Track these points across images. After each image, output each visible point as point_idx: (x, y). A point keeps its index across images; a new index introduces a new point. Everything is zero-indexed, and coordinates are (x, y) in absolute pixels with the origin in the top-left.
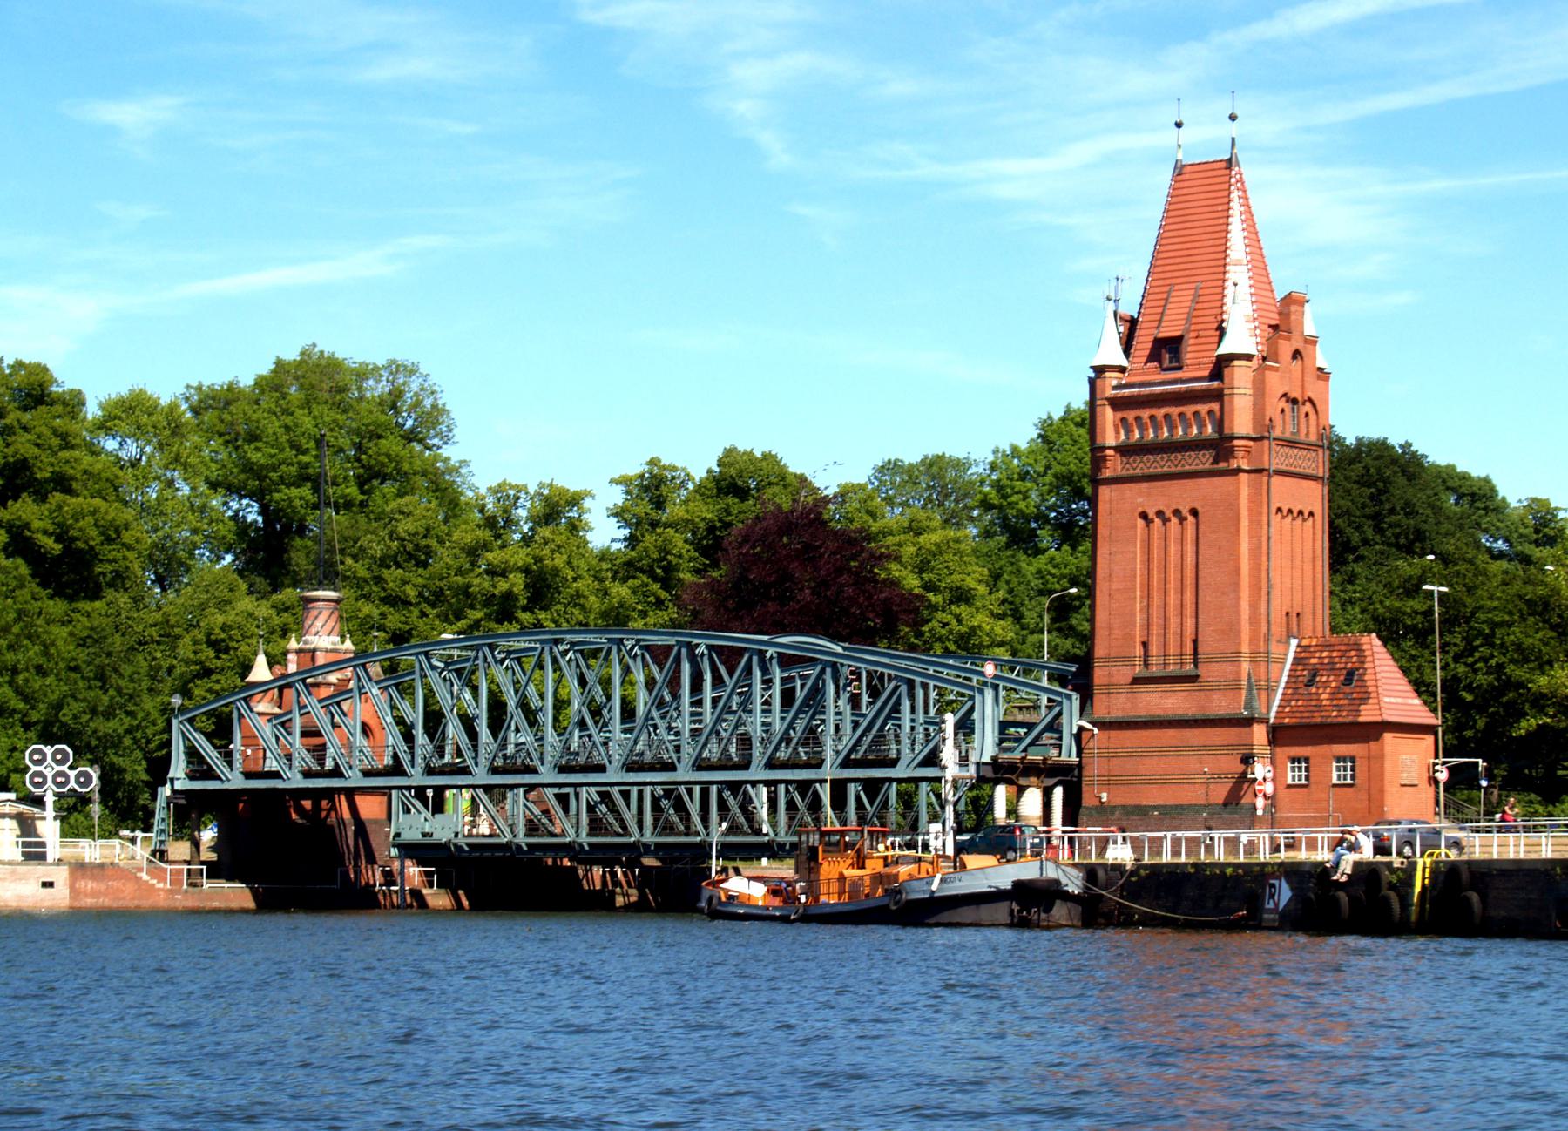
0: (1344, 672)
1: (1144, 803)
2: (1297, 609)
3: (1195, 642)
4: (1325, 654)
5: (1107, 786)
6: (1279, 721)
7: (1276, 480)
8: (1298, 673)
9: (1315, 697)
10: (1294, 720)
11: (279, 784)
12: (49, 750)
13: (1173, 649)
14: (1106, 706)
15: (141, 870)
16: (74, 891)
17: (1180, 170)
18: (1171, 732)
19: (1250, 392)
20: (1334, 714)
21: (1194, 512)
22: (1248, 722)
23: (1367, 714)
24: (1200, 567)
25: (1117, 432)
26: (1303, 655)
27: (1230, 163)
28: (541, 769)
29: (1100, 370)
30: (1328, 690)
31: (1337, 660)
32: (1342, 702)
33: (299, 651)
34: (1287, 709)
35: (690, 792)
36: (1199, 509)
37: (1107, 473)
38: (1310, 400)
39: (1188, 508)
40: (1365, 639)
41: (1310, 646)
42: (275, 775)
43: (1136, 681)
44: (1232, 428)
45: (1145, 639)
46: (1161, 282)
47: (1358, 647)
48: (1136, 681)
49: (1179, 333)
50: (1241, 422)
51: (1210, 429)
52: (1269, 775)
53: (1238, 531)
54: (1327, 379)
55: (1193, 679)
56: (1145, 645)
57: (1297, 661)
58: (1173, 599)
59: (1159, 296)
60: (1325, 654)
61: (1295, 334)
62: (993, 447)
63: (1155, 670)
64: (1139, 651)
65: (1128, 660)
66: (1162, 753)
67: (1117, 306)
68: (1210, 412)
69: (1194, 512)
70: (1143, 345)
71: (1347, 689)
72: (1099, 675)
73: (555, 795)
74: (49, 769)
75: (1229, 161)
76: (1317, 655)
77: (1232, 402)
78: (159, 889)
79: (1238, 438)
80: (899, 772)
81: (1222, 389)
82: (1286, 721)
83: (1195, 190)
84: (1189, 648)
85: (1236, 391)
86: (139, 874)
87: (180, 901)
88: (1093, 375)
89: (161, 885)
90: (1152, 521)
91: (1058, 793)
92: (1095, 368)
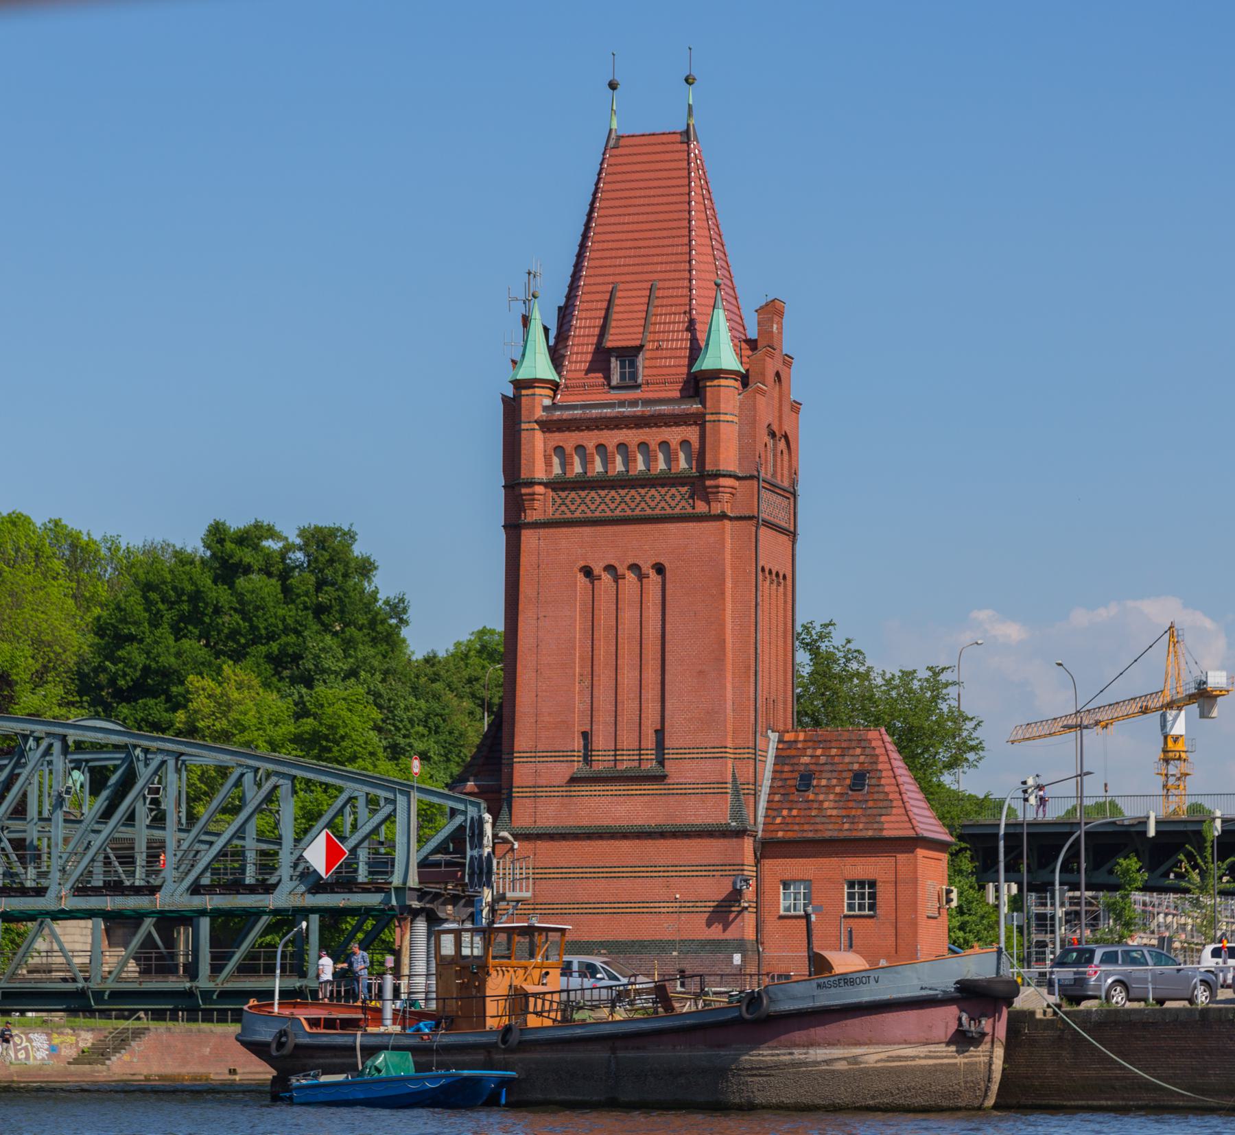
1: (586, 939)
2: (773, 696)
3: (660, 733)
6: (768, 835)
7: (764, 533)
8: (785, 776)
13: (628, 740)
14: (524, 814)
17: (614, 144)
20: (846, 826)
21: (660, 569)
23: (892, 828)
24: (668, 637)
25: (549, 464)
26: (788, 753)
30: (832, 797)
31: (837, 760)
34: (778, 820)
36: (667, 565)
37: (531, 516)
38: (786, 437)
39: (650, 563)
40: (872, 734)
41: (796, 742)
43: (573, 780)
44: (716, 461)
45: (587, 728)
48: (573, 780)
50: (727, 457)
51: (683, 464)
53: (723, 593)
55: (661, 778)
56: (585, 735)
58: (628, 677)
60: (819, 752)
63: (599, 767)
64: (578, 743)
65: (562, 755)
66: (612, 874)
68: (685, 443)
69: (660, 569)
70: (580, 351)
71: (858, 796)
72: (522, 773)
75: (687, 133)
79: (724, 476)
80: (161, 901)
81: (704, 415)
82: (780, 834)
84: (650, 741)
85: (722, 417)
90: (599, 578)
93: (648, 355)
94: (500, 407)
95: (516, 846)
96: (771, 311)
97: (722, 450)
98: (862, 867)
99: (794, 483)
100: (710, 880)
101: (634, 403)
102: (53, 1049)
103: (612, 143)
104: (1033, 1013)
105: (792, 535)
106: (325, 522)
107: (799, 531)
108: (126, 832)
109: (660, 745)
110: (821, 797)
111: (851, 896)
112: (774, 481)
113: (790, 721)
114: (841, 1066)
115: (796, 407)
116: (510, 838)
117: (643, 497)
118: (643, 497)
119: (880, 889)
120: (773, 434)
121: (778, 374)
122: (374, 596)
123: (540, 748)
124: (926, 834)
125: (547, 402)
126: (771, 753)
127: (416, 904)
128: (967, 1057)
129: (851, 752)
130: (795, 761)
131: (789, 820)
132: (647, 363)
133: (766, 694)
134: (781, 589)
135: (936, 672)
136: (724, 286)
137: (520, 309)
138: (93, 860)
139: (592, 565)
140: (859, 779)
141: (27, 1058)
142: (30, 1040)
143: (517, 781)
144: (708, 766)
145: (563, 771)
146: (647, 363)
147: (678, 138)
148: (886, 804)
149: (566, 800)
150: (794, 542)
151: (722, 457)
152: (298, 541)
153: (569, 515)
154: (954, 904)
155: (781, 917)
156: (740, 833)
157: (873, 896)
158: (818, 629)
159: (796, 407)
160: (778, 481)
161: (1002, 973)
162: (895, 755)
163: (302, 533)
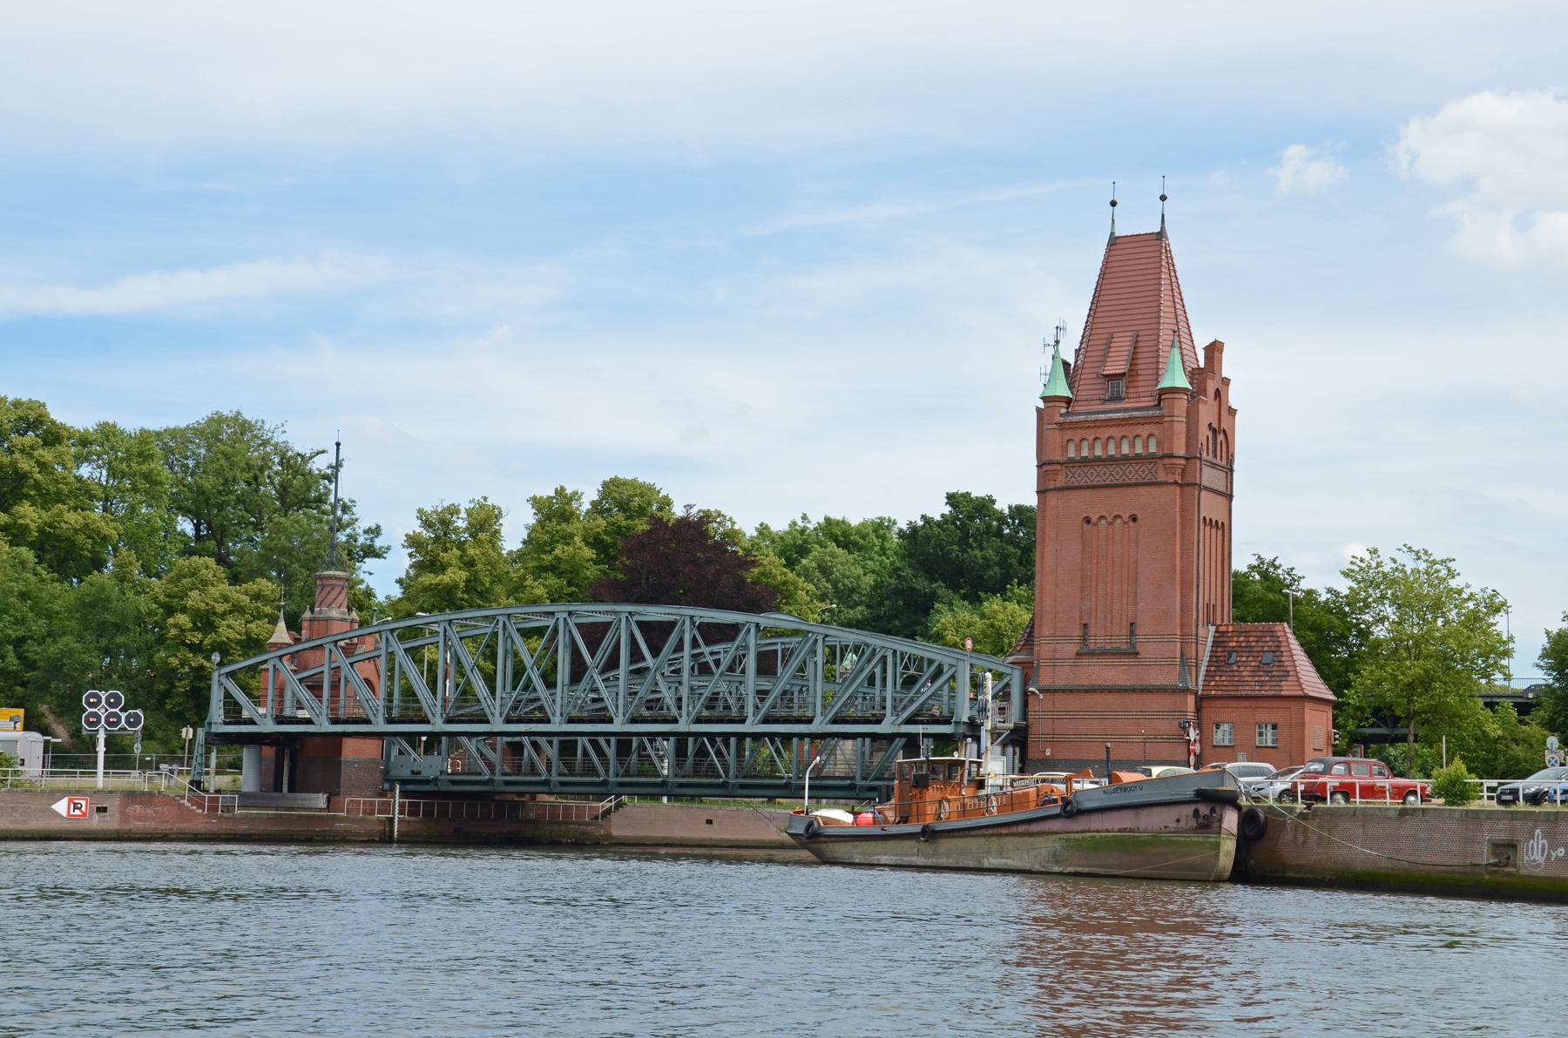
4: (1242, 639)
5: (1051, 742)
6: (1206, 693)
7: (1204, 493)
9: (1237, 674)
12: (103, 695)
15: (183, 797)
16: (124, 816)
17: (1114, 241)
18: (1110, 698)
22: (1185, 691)
26: (1222, 639)
27: (1161, 235)
30: (1248, 668)
31: (1253, 644)
32: (1263, 678)
34: (1213, 683)
35: (608, 742)
38: (1224, 431)
41: (1227, 632)
42: (309, 722)
47: (1272, 633)
52: (1198, 738)
57: (1216, 643)
59: (1096, 337)
60: (1242, 639)
61: (1217, 377)
62: (1505, 594)
67: (1057, 351)
74: (103, 710)
76: (1235, 639)
77: (1172, 428)
78: (199, 814)
82: (1213, 692)
86: (181, 801)
88: (1041, 405)
91: (1017, 750)
92: (1045, 399)
95: (1041, 697)
97: (1175, 440)
99: (1230, 461)
100: (1165, 721)
105: (1230, 497)
108: (765, 684)
110: (1242, 669)
112: (1214, 461)
116: (1037, 692)
117: (1124, 472)
118: (1124, 472)
120: (1214, 431)
124: (1311, 694)
125: (1063, 411)
126: (1210, 639)
129: (1263, 639)
130: (1226, 644)
131: (1219, 683)
133: (1207, 601)
134: (1220, 532)
136: (1181, 333)
137: (1051, 351)
138: (617, 707)
139: (1091, 516)
147: (1155, 236)
148: (1285, 674)
151: (1175, 445)
153: (1115, 482)
156: (1185, 691)
159: (1232, 412)
160: (1218, 461)
161: (344, 739)
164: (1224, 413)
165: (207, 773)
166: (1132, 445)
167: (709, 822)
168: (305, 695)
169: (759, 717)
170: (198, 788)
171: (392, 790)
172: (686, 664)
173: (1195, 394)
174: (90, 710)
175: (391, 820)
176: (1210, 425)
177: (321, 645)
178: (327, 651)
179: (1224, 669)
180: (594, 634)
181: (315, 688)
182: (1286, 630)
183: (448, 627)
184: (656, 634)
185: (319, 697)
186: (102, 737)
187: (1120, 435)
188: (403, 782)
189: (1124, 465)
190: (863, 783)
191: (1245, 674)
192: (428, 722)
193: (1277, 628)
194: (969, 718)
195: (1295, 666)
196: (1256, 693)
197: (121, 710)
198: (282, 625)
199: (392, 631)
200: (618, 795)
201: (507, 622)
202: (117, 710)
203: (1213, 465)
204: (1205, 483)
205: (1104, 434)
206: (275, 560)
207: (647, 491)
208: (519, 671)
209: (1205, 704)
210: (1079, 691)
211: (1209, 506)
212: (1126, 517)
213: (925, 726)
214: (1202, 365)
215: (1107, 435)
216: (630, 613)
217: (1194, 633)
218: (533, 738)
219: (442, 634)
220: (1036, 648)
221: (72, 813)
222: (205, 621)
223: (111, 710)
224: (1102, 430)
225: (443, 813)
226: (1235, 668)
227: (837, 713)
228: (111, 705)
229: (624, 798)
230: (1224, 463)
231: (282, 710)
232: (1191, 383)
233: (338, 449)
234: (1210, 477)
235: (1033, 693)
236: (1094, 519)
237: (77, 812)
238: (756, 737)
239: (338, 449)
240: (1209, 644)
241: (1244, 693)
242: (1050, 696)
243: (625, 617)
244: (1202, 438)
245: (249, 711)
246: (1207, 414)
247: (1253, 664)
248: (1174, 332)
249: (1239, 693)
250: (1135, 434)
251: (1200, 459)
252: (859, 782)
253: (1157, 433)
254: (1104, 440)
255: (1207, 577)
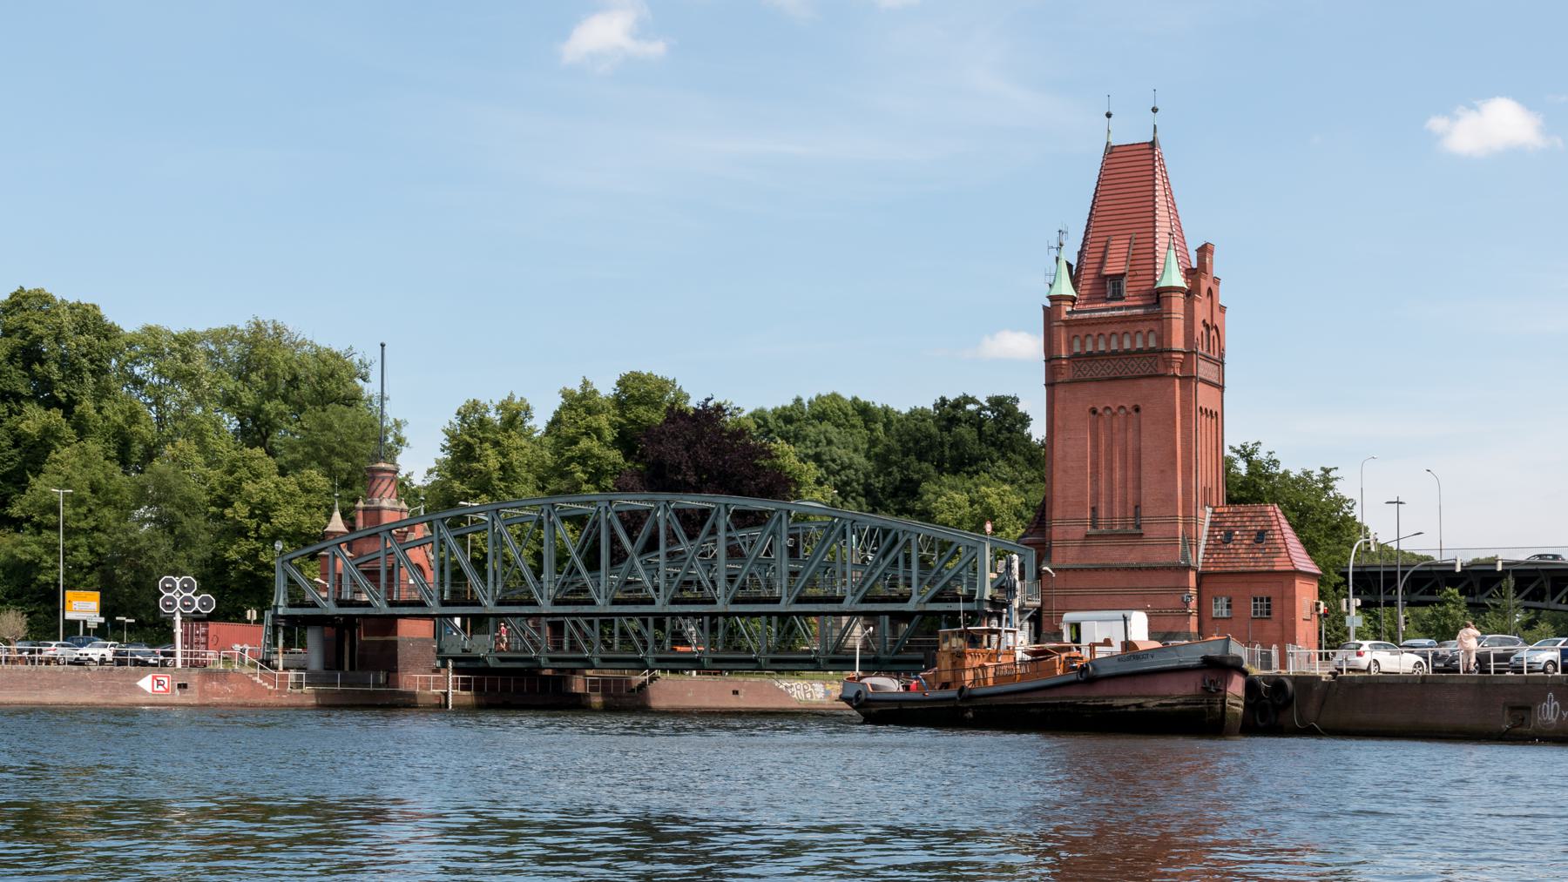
0: (1255, 533)
6: (1205, 569)
7: (1200, 385)
10: (1218, 569)
11: (370, 611)
12: (178, 581)
17: (1111, 151)
19: (1182, 317)
23: (1280, 565)
27: (1153, 145)
28: (598, 601)
29: (1056, 300)
33: (365, 510)
34: (1211, 560)
38: (1216, 328)
42: (368, 604)
46: (1100, 234)
47: (1264, 514)
49: (1122, 272)
53: (1175, 422)
54: (1224, 312)
56: (1093, 509)
57: (1213, 524)
59: (1100, 244)
60: (1236, 519)
61: (1209, 277)
65: (1080, 521)
73: (549, 622)
74: (178, 595)
76: (1231, 519)
77: (1170, 325)
78: (270, 691)
83: (1125, 165)
86: (254, 679)
87: (285, 699)
88: (1048, 304)
89: (271, 687)
91: (1033, 624)
92: (1051, 298)
93: (1129, 279)
94: (1042, 312)
96: (1204, 250)
98: (1261, 590)
99: (1222, 355)
101: (1120, 308)
102: (827, 693)
103: (1108, 151)
104: (1320, 677)
105: (1221, 388)
106: (999, 393)
107: (1226, 385)
109: (1137, 515)
110: (1237, 547)
111: (1256, 606)
112: (1208, 354)
113: (1220, 501)
114: (1133, 709)
115: (1223, 309)
119: (1273, 602)
120: (1207, 326)
121: (1210, 289)
122: (1030, 436)
123: (1068, 517)
124: (1301, 569)
125: (1069, 309)
126: (1208, 520)
127: (989, 610)
128: (186, 697)
132: (1129, 284)
134: (1214, 420)
135: (1327, 471)
136: (1177, 234)
137: (1054, 253)
140: (1261, 536)
141: (812, 697)
142: (813, 687)
143: (1054, 537)
144: (1167, 527)
145: (1079, 531)
146: (1129, 284)
147: (1148, 146)
148: (1276, 550)
149: (1083, 548)
150: (1223, 392)
152: (987, 404)
153: (1082, 377)
154: (1322, 611)
155: (1214, 618)
157: (1268, 606)
158: (1251, 447)
159: (1223, 309)
160: (1211, 355)
161: (399, 620)
162: (1283, 521)
163: (989, 400)
164: (1216, 310)
165: (276, 653)
166: (1133, 341)
167: (736, 692)
168: (363, 581)
169: (792, 598)
170: (268, 665)
171: (445, 666)
172: (721, 550)
173: (1189, 294)
174: (166, 594)
175: (446, 695)
176: (1204, 321)
177: (376, 534)
178: (382, 539)
179: (1221, 547)
180: (633, 521)
181: (372, 575)
182: (1274, 510)
183: (495, 516)
184: (693, 522)
185: (378, 587)
186: (178, 618)
187: (1122, 331)
188: (455, 659)
189: (1151, 357)
190: (886, 656)
191: (1240, 551)
192: (480, 605)
193: (1269, 508)
194: (991, 596)
195: (1285, 544)
196: (1252, 569)
197: (195, 594)
198: (337, 515)
199: (443, 520)
200: (651, 670)
201: (552, 512)
202: (190, 594)
203: (1207, 359)
204: (1200, 375)
205: (1108, 330)
206: (320, 455)
207: (663, 385)
208: (562, 558)
209: (1204, 580)
210: (1111, 569)
211: (1205, 396)
212: (1129, 407)
213: (949, 604)
214: (1194, 265)
215: (1110, 331)
216: (668, 502)
217: (1194, 514)
218: (574, 619)
219: (490, 524)
220: (1048, 530)
221: (156, 689)
222: (264, 511)
223: (185, 594)
224: (1105, 326)
225: (492, 688)
226: (1231, 546)
227: (865, 594)
228: (185, 589)
229: (658, 673)
230: (1216, 356)
231: (340, 594)
232: (1187, 283)
233: (383, 350)
234: (1204, 370)
235: (1046, 571)
236: (1100, 410)
237: (161, 688)
238: (727, 615)
239: (383, 350)
240: (1207, 524)
241: (1241, 569)
242: (1062, 575)
243: (662, 507)
244: (1197, 334)
245: (312, 594)
246: (1201, 311)
247: (1247, 542)
248: (1170, 234)
249: (1236, 569)
250: (1136, 330)
251: (1196, 353)
252: (883, 656)
253: (1156, 329)
254: (1107, 336)
255: (1204, 462)
